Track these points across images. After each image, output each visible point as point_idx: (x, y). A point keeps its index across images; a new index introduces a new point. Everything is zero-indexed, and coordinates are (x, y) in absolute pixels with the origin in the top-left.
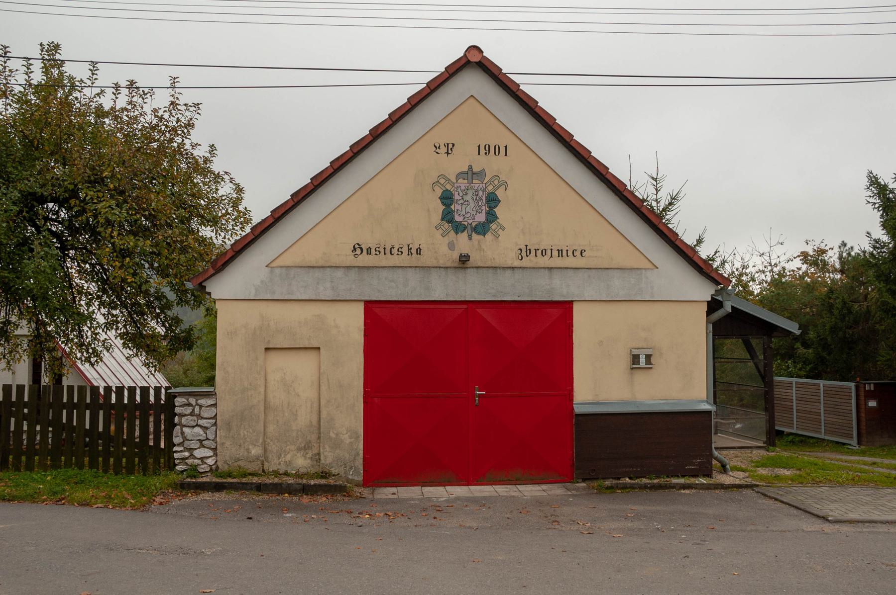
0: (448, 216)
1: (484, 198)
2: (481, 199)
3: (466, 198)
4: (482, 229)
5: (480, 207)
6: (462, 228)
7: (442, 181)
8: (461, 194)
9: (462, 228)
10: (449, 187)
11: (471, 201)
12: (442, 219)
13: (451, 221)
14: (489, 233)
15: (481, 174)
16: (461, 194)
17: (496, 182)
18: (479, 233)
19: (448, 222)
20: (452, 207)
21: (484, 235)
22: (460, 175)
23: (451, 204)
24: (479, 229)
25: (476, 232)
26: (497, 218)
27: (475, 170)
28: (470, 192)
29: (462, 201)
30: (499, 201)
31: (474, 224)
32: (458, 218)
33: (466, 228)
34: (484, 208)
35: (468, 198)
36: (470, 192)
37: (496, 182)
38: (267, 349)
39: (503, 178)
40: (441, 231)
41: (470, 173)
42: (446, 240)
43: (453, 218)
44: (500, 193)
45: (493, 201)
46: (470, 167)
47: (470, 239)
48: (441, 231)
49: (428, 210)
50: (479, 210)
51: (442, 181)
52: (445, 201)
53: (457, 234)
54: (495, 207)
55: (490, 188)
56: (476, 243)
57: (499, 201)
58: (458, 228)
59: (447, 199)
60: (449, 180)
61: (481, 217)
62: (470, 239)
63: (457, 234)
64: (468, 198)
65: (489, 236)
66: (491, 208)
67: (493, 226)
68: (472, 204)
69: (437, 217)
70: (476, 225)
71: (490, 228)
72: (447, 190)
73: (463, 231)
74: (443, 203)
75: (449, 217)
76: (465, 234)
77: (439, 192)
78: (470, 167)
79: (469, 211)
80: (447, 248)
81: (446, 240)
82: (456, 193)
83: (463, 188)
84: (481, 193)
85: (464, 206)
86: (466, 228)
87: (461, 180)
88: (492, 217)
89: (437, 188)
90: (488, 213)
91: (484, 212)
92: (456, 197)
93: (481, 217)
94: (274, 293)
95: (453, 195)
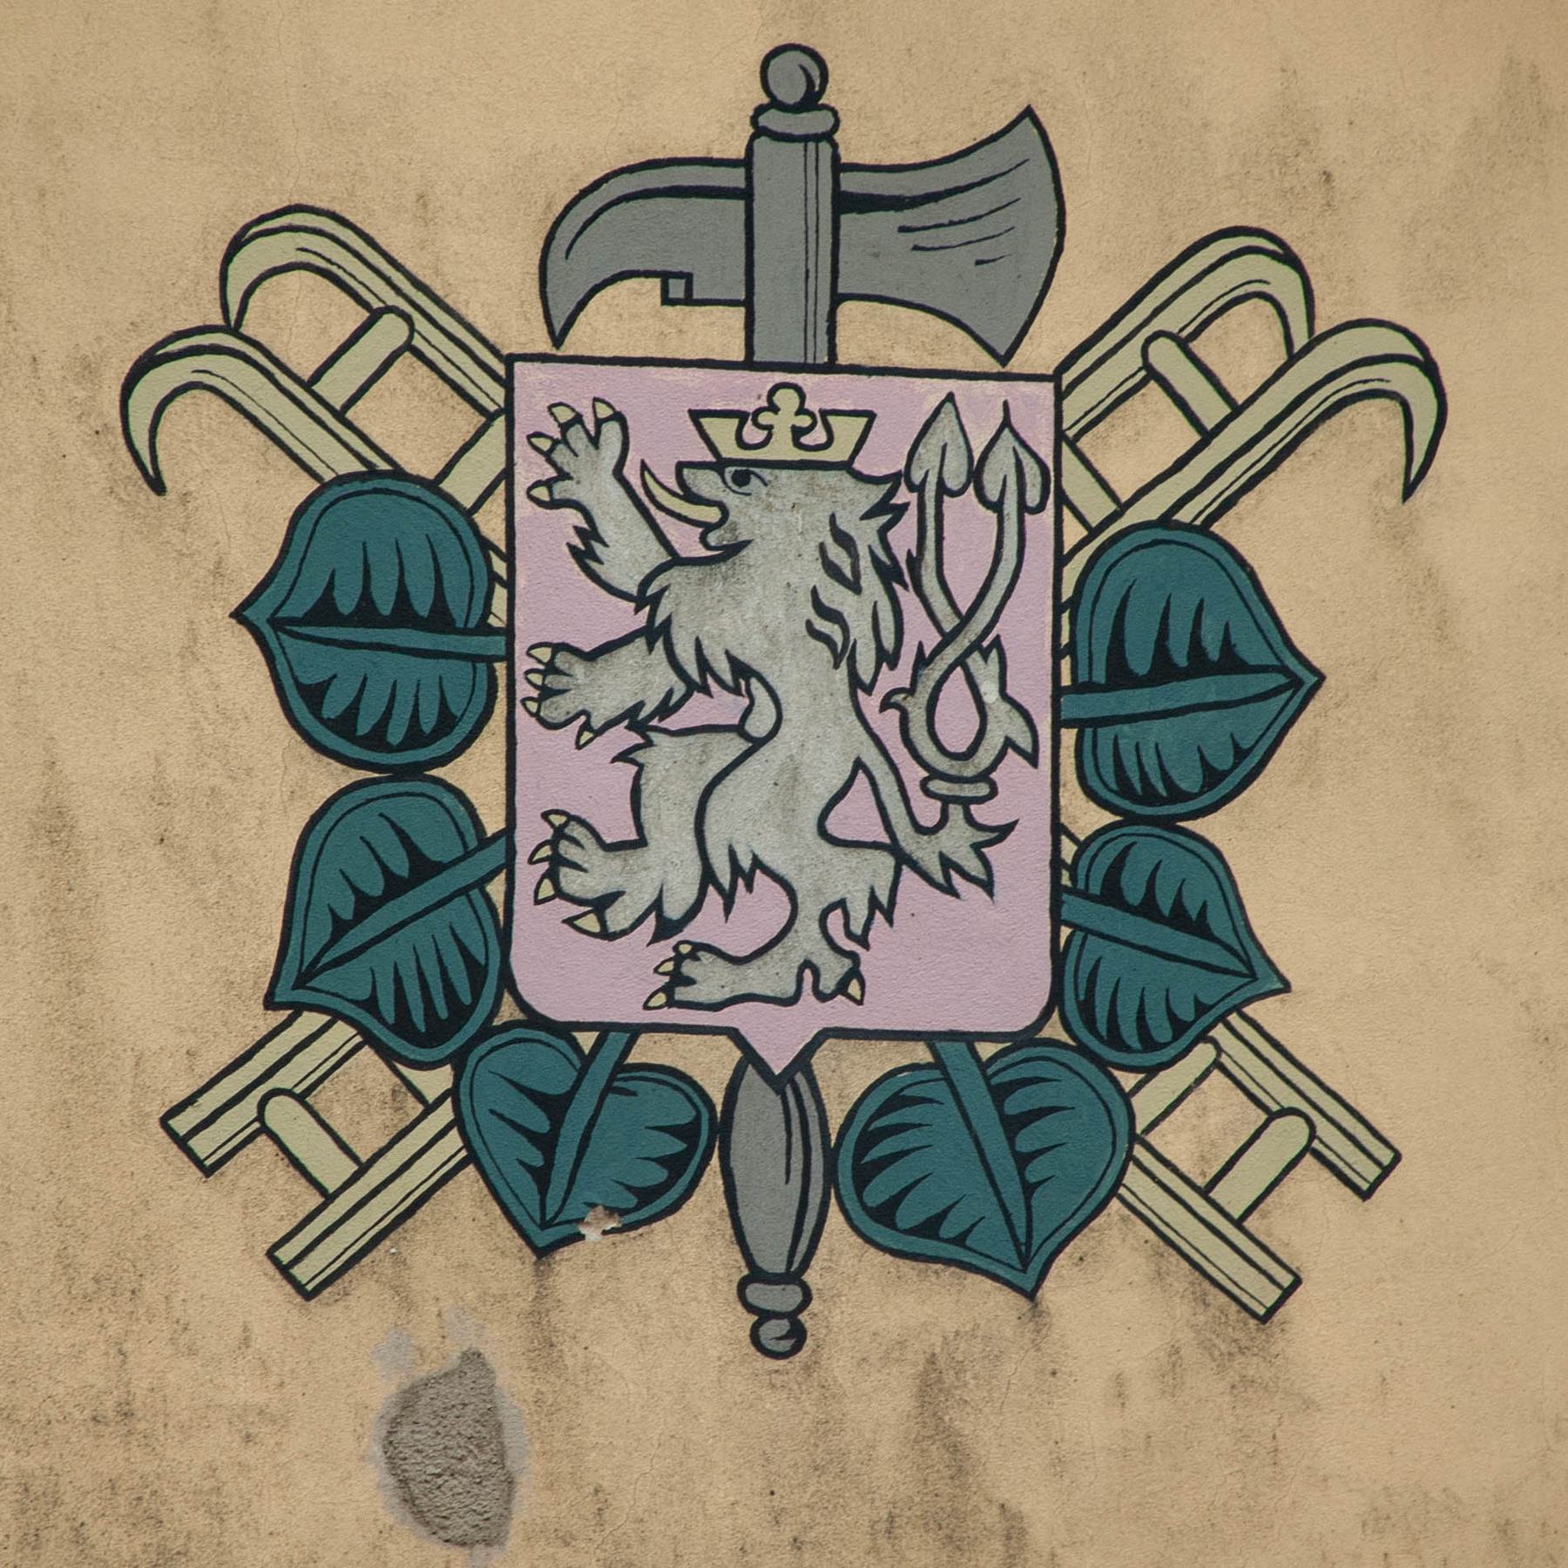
0: (392, 939)
1: (1028, 628)
2: (973, 639)
3: (714, 617)
4: (983, 1165)
5: (963, 783)
6: (629, 1141)
7: (301, 319)
8: (629, 551)
9: (629, 1141)
10: (413, 425)
11: (804, 679)
12: (295, 985)
13: (445, 1015)
14: (1114, 1240)
15: (983, 203)
16: (629, 551)
17: (1245, 349)
18: (916, 1235)
19: (410, 1029)
20: (476, 773)
21: (1024, 1266)
22: (609, 220)
23: (452, 730)
24: (944, 1164)
25: (881, 1223)
26: (1254, 973)
27: (884, 123)
28: (786, 529)
29: (640, 678)
30: (1298, 683)
31: (846, 1079)
32: (568, 973)
33: (701, 1136)
34: (1021, 793)
35: (753, 612)
36: (786, 529)
37: (1245, 349)
38: (979, 263)
39: (1366, 275)
40: (263, 1196)
41: (781, 171)
42: (355, 1355)
43: (491, 969)
44: (1305, 544)
45: (1181, 675)
46: (797, 92)
47: (779, 1321)
48: (263, 1196)
49: (54, 825)
50: (930, 829)
51: (301, 319)
52: (339, 668)
53: (546, 1235)
54: (1228, 778)
55: (1139, 450)
56: (879, 1408)
57: (1298, 683)
58: (575, 1141)
59: (378, 626)
60: (419, 299)
61: (978, 963)
62: (779, 1321)
63: (546, 1235)
64: (753, 612)
65: (1109, 1293)
66: (1155, 804)
67: (1191, 1116)
68: (819, 734)
69: (191, 951)
70: (891, 1101)
71: (1131, 1139)
72: (381, 479)
73: (647, 1205)
74: (309, 708)
75: (410, 949)
76: (685, 1261)
77: (242, 501)
78: (797, 92)
79: (770, 837)
80: (368, 1490)
81: (355, 1355)
82: (544, 538)
83: (664, 443)
84: (969, 531)
85: (674, 769)
86: (701, 1136)
87: (624, 318)
88: (1158, 950)
89: (198, 439)
90: (1087, 887)
91: (1024, 867)
92: (550, 601)
93: (978, 963)
94: (299, 663)
95: (493, 565)
